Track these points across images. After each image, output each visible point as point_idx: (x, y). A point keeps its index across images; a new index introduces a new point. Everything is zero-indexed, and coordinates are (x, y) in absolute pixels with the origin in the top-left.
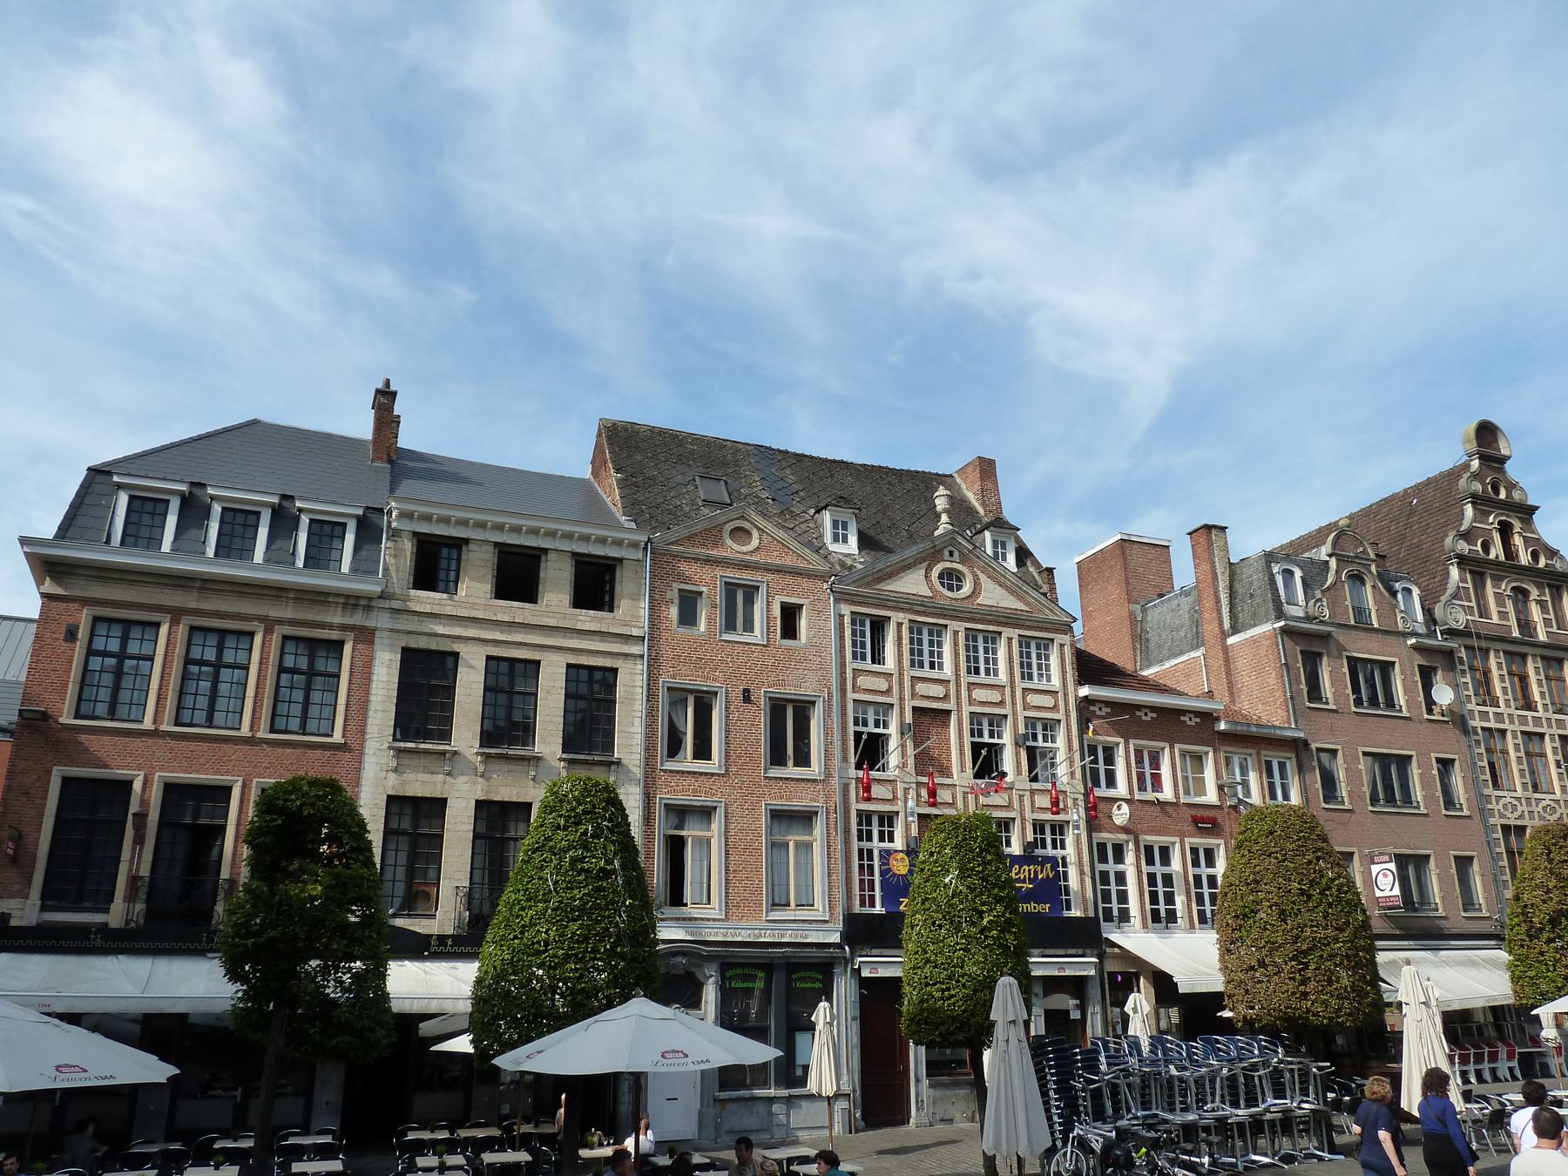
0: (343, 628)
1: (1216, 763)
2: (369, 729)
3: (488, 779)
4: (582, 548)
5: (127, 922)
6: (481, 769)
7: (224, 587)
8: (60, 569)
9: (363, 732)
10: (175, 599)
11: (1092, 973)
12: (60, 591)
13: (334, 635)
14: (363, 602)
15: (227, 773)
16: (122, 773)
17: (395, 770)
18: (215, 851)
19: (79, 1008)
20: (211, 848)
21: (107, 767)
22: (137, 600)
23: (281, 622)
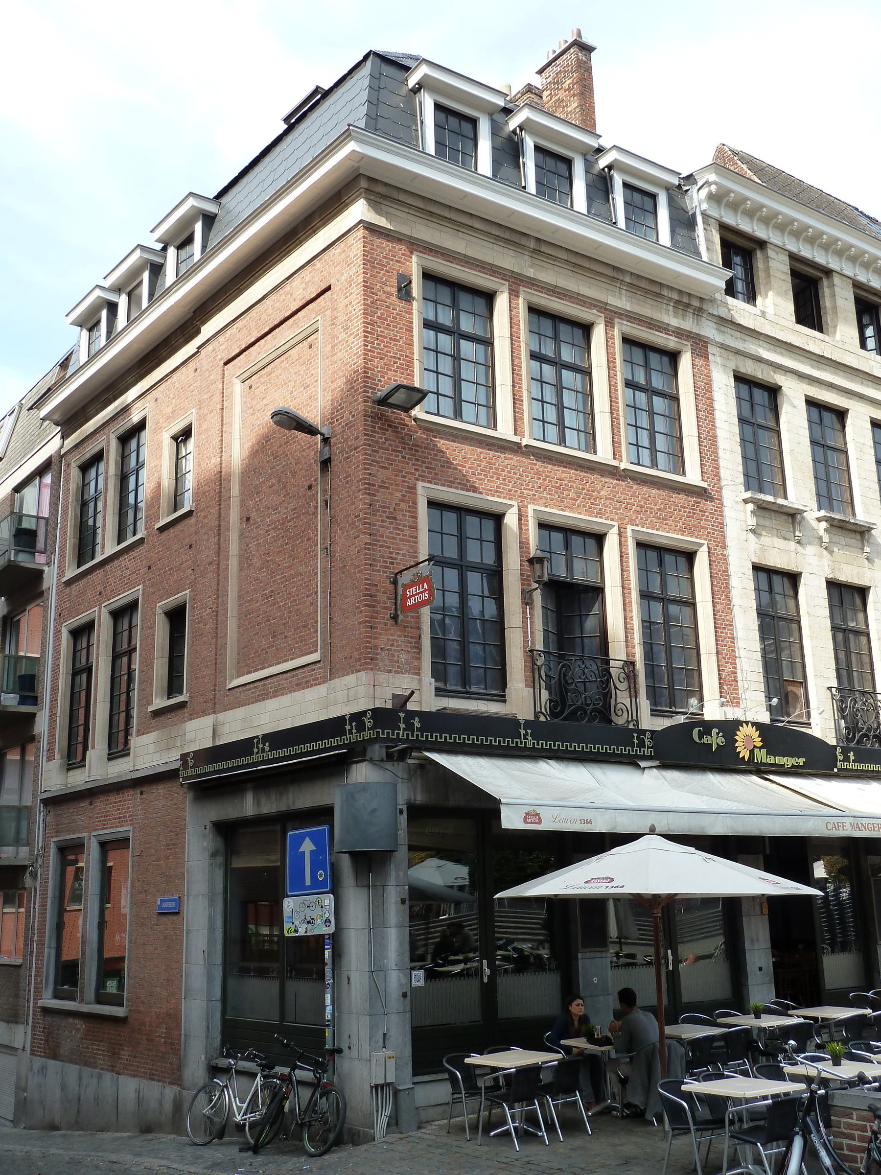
0: (680, 333)
1: (608, 339)
2: (723, 473)
3: (831, 552)
4: (806, 252)
5: (536, 715)
6: (826, 538)
7: (477, 224)
8: (381, 189)
9: (717, 475)
10: (621, 301)
11: (279, 864)
12: (381, 222)
13: (671, 343)
14: (696, 303)
15: (600, 514)
16: (491, 500)
17: (753, 531)
18: (590, 623)
19: (719, 828)
20: (582, 618)
21: (475, 489)
22: (471, 253)
23: (532, 283)
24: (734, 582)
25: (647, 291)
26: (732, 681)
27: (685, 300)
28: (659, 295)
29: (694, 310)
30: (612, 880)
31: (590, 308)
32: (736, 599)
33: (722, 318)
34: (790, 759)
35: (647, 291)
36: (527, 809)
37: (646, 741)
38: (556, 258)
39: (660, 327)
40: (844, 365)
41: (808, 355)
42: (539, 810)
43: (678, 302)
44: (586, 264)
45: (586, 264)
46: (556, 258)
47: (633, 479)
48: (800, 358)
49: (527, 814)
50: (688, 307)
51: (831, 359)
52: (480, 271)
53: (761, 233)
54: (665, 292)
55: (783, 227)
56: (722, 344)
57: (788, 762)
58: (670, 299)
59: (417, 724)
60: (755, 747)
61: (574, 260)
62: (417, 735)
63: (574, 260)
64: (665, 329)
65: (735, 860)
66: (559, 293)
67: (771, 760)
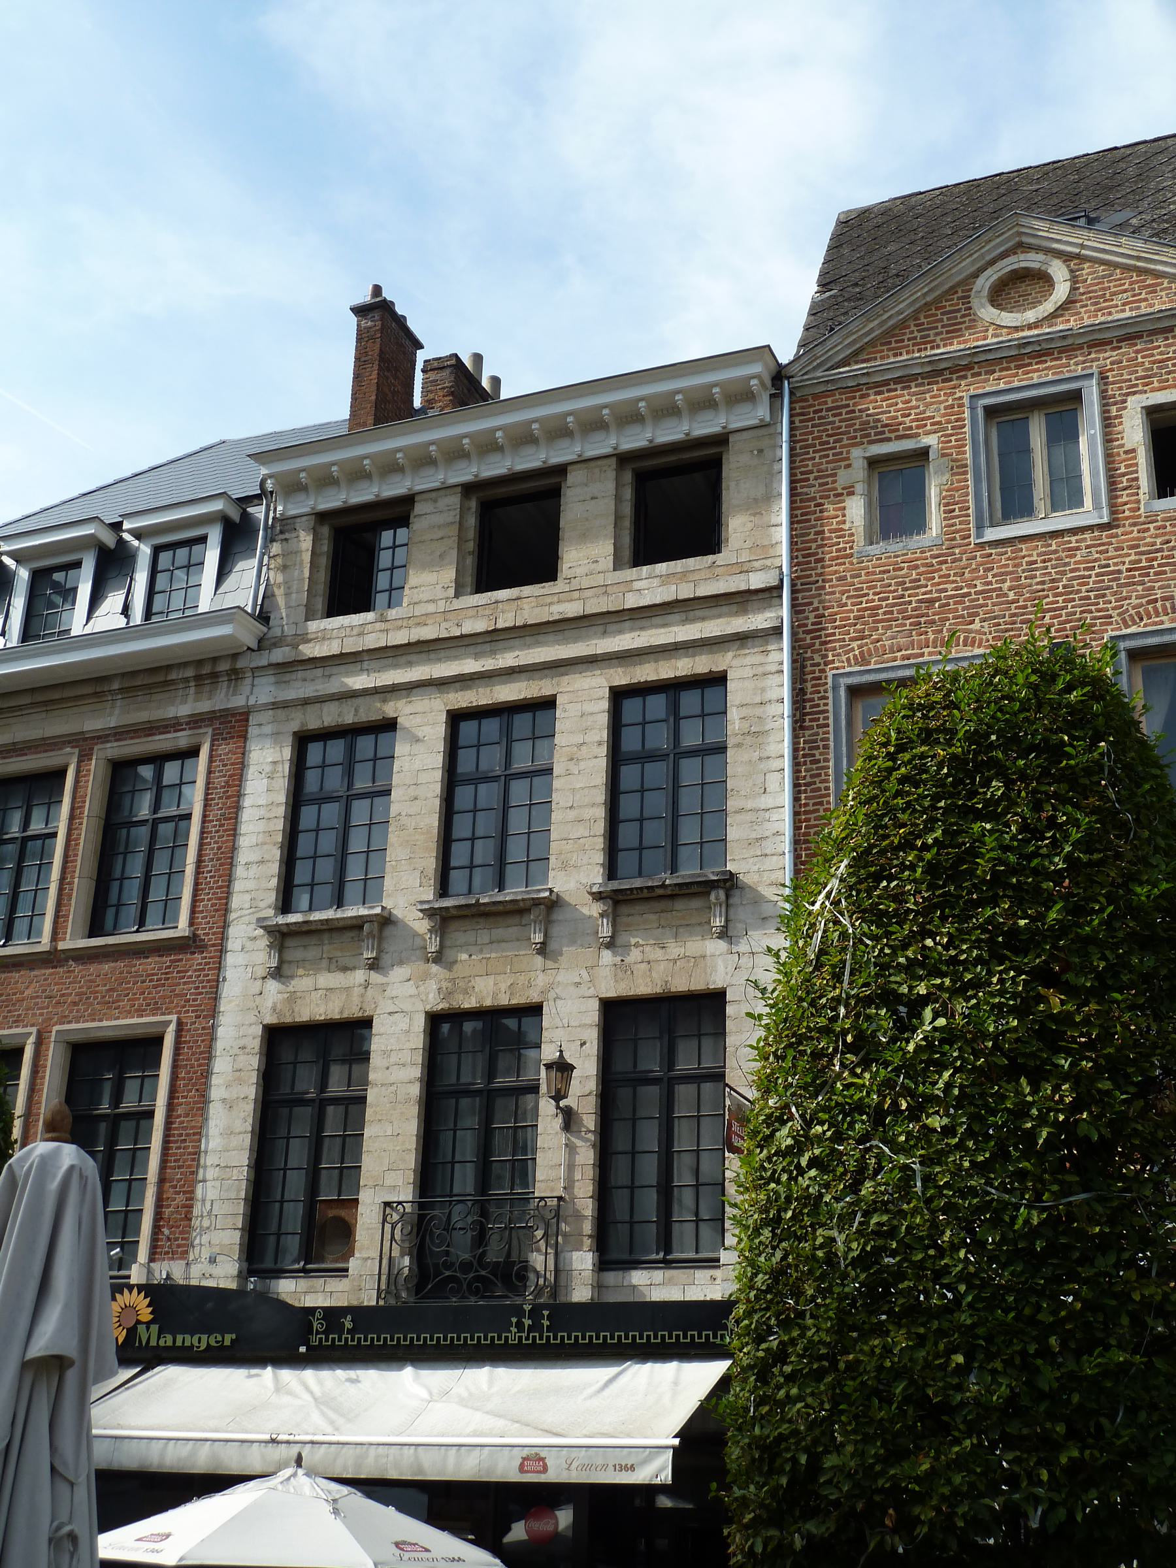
4: (635, 439)
14: (224, 666)
24: (221, 1066)
25: (149, 686)
26: (182, 1220)
27: (206, 670)
28: (166, 683)
29: (228, 675)
30: (427, 1550)
31: (61, 749)
32: (218, 1090)
33: (278, 664)
34: (204, 1337)
35: (149, 686)
36: (526, 1452)
37: (315, 1324)
38: (20, 708)
39: (166, 726)
40: (548, 623)
41: (466, 641)
42: (543, 1453)
43: (198, 678)
44: (56, 695)
45: (56, 695)
46: (20, 708)
47: (75, 959)
48: (453, 652)
49: (524, 1459)
50: (218, 677)
51: (609, 613)
52: (132, 738)
53: (706, 426)
54: (173, 676)
55: (423, 460)
56: (273, 703)
57: (201, 1341)
58: (186, 680)
59: (348, 1325)
60: (138, 1322)
61: (40, 698)
62: (346, 1339)
63: (40, 698)
64: (174, 725)
65: (443, 1529)
66: (22, 749)
67: (167, 1341)
